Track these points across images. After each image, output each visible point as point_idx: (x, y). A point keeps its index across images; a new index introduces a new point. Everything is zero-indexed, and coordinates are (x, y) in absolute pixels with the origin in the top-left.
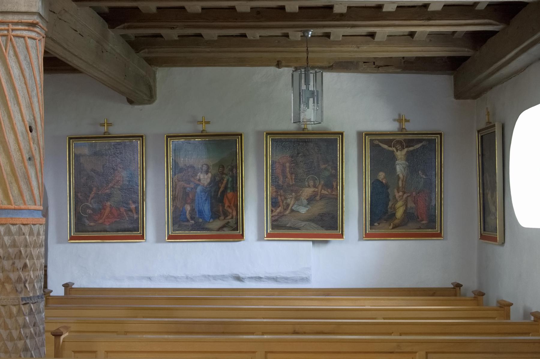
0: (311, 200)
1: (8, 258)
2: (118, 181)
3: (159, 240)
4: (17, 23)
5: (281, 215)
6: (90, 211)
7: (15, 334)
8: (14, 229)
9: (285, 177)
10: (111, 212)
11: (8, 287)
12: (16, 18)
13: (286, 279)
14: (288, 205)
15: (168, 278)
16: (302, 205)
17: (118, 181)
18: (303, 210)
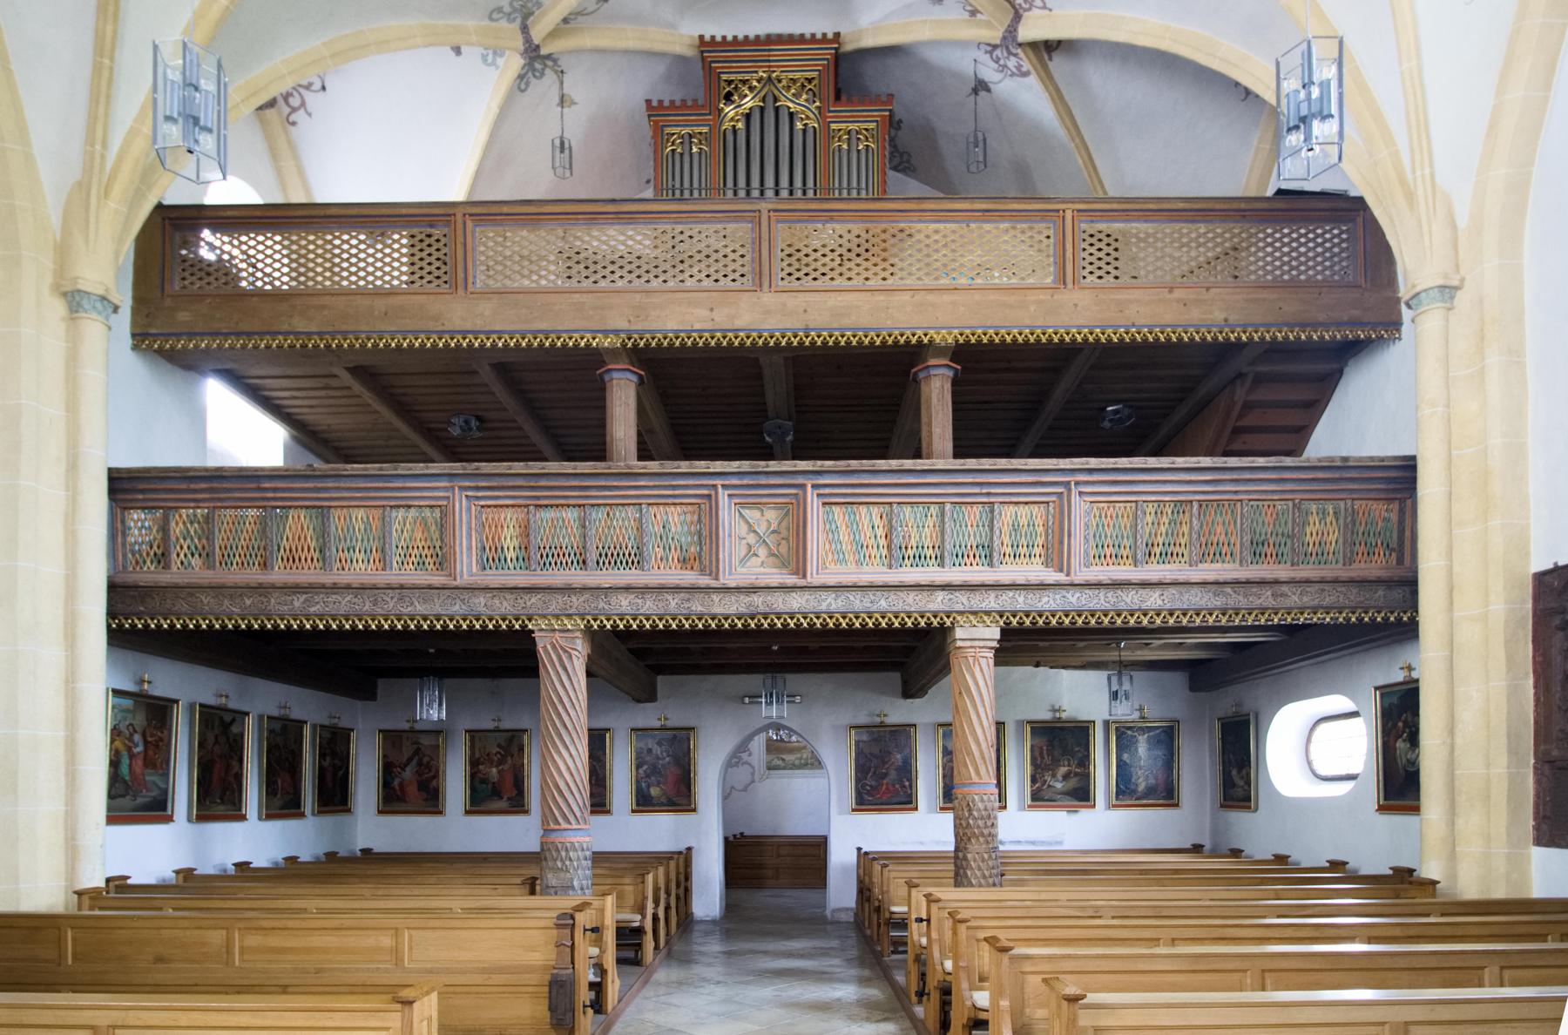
0: (1066, 777)
1: (982, 818)
2: (893, 763)
3: (930, 811)
4: (980, 647)
5: (1039, 790)
6: (868, 788)
7: (987, 873)
8: (985, 797)
9: (1042, 758)
10: (887, 789)
11: (981, 839)
12: (982, 644)
13: (1043, 843)
14: (1045, 781)
15: (938, 843)
16: (1057, 781)
17: (893, 763)
18: (1059, 785)
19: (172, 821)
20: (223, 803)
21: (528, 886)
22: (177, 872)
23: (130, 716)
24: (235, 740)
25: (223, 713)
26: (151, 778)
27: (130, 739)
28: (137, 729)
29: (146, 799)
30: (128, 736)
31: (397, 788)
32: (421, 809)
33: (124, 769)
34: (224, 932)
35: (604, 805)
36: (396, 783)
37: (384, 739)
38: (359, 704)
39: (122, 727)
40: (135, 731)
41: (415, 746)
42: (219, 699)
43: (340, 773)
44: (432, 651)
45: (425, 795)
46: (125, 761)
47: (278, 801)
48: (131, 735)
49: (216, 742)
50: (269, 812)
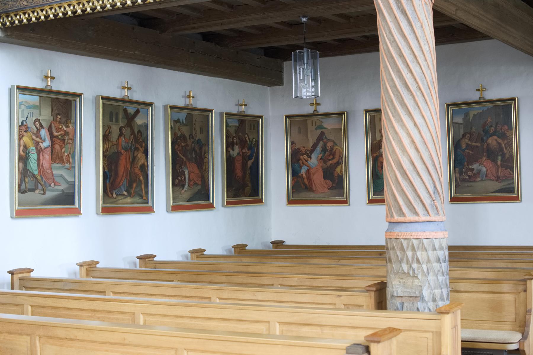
19: (153, 211)
20: (130, 195)
21: (373, 294)
22: (81, 265)
23: (36, 112)
24: (139, 132)
25: (126, 105)
26: (58, 171)
27: (38, 135)
28: (43, 124)
29: (56, 193)
30: (35, 132)
31: (304, 176)
32: (327, 198)
33: (33, 165)
34: (29, 338)
35: (512, 190)
36: (303, 171)
37: (291, 122)
38: (268, 90)
39: (30, 123)
40: (42, 126)
41: (319, 132)
42: (188, 100)
43: (250, 163)
44: (304, 20)
45: (329, 182)
46: (34, 156)
47: (186, 192)
48: (38, 130)
49: (121, 134)
50: (176, 204)
